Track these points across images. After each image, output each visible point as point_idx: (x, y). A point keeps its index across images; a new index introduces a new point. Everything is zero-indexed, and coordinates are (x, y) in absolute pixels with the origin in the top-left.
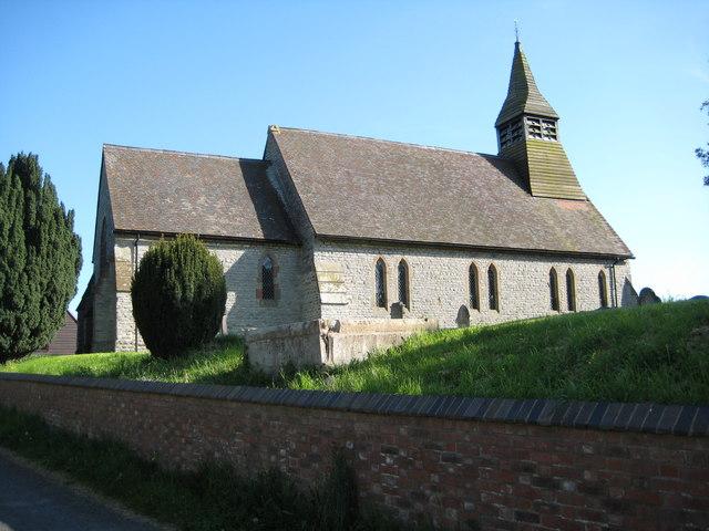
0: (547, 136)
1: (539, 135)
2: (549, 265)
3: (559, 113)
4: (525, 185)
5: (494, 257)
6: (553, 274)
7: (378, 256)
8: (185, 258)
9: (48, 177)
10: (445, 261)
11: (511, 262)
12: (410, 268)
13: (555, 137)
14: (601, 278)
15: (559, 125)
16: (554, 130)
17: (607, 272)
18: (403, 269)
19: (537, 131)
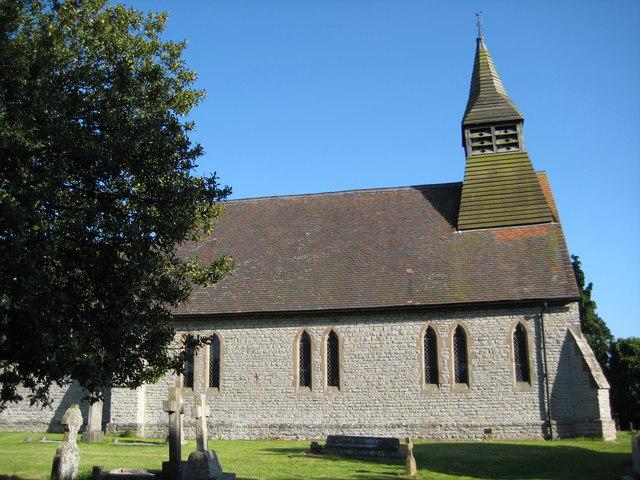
0: (503, 146)
1: (490, 147)
2: (517, 319)
3: (522, 115)
4: (454, 221)
5: (336, 322)
6: (431, 338)
7: (187, 333)
8: (129, 442)
9: (149, 471)
10: (267, 332)
11: (492, 319)
12: (223, 343)
13: (516, 145)
14: (521, 334)
15: (524, 133)
16: (515, 136)
17: (530, 326)
18: (461, 337)
19: (486, 143)
